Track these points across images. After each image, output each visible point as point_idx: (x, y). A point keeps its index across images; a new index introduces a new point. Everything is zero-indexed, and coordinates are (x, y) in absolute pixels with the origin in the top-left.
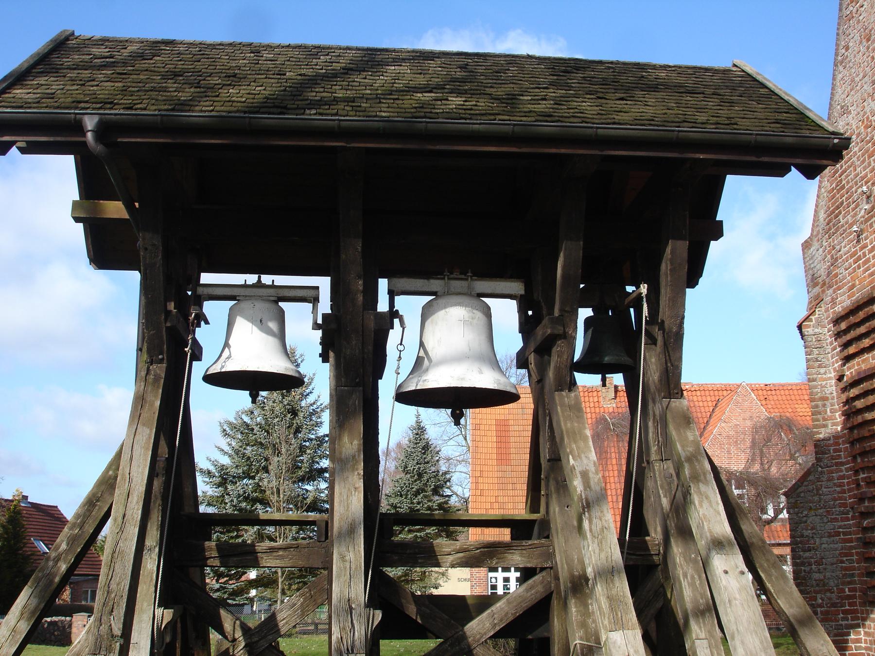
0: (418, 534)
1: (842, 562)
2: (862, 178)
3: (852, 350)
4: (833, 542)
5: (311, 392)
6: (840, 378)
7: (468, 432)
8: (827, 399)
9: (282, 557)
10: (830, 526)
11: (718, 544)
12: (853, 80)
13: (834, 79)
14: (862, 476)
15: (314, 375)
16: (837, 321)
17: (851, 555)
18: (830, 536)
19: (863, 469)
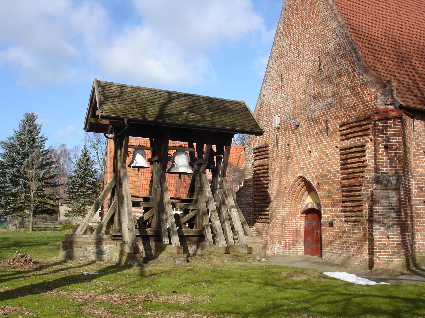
0: (85, 193)
1: (248, 211)
2: (266, 115)
3: (257, 158)
4: (247, 206)
5: (40, 132)
6: (253, 164)
7: (99, 151)
8: (249, 169)
9: (145, 205)
10: (246, 202)
11: (233, 207)
12: (267, 89)
13: (262, 86)
14: (256, 190)
15: (41, 125)
16: (254, 150)
17: (251, 210)
18: (246, 204)
19: (256, 189)
